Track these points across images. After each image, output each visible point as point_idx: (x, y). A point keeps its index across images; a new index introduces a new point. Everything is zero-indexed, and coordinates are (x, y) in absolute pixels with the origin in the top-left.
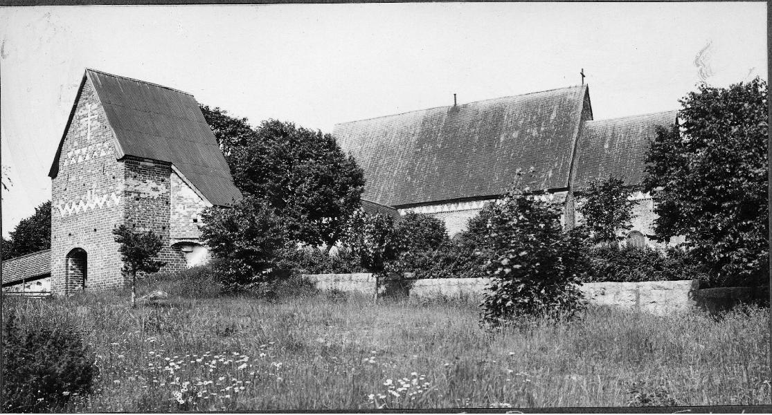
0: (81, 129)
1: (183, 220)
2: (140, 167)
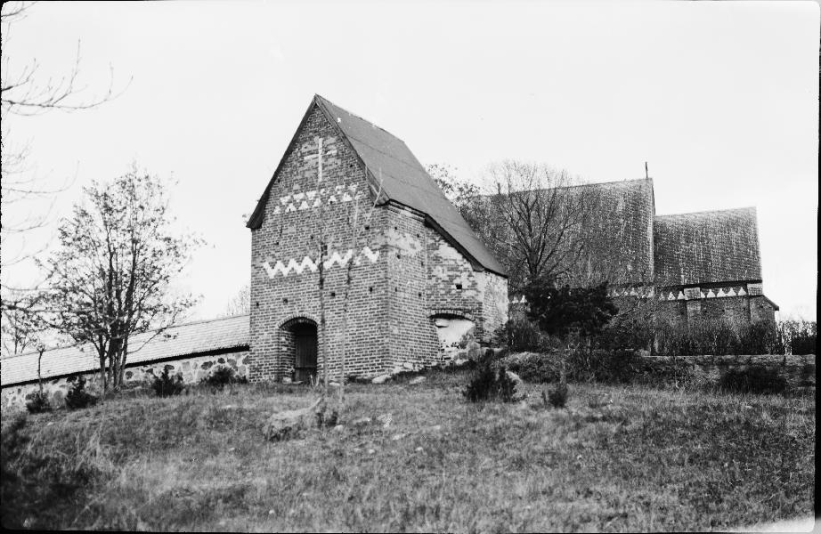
1: (442, 286)
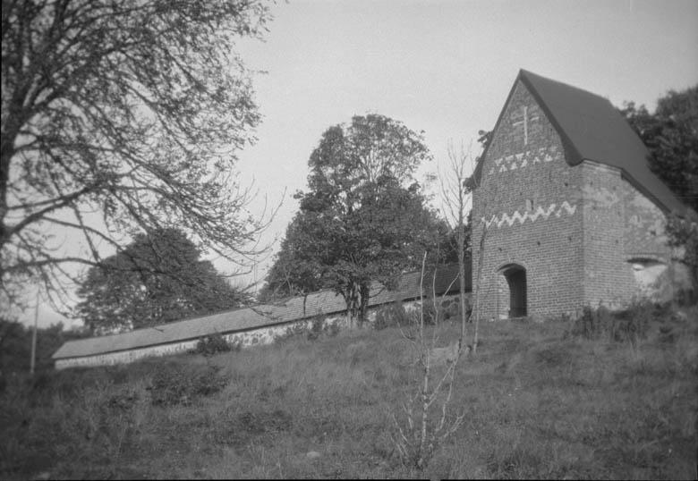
2: (595, 173)
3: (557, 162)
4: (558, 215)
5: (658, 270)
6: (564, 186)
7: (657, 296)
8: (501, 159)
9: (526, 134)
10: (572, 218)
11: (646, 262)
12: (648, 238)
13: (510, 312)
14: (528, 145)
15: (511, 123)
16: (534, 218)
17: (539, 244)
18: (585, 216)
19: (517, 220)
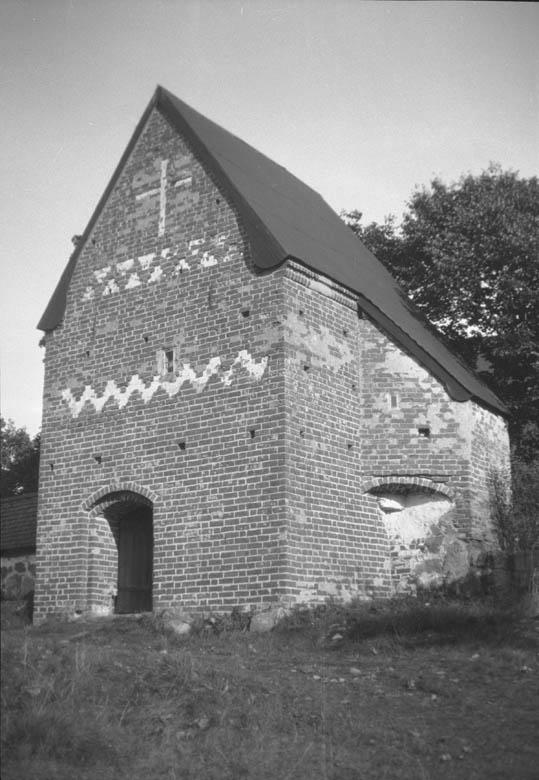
0: (136, 216)
2: (309, 292)
3: (226, 268)
4: (226, 381)
5: (434, 511)
6: (240, 317)
7: (431, 566)
8: (108, 269)
9: (163, 214)
10: (256, 386)
11: (407, 493)
12: (414, 441)
13: (116, 599)
14: (166, 235)
15: (132, 196)
16: (172, 389)
17: (182, 446)
18: (286, 382)
19: (136, 394)
